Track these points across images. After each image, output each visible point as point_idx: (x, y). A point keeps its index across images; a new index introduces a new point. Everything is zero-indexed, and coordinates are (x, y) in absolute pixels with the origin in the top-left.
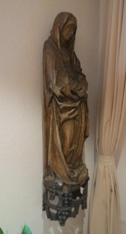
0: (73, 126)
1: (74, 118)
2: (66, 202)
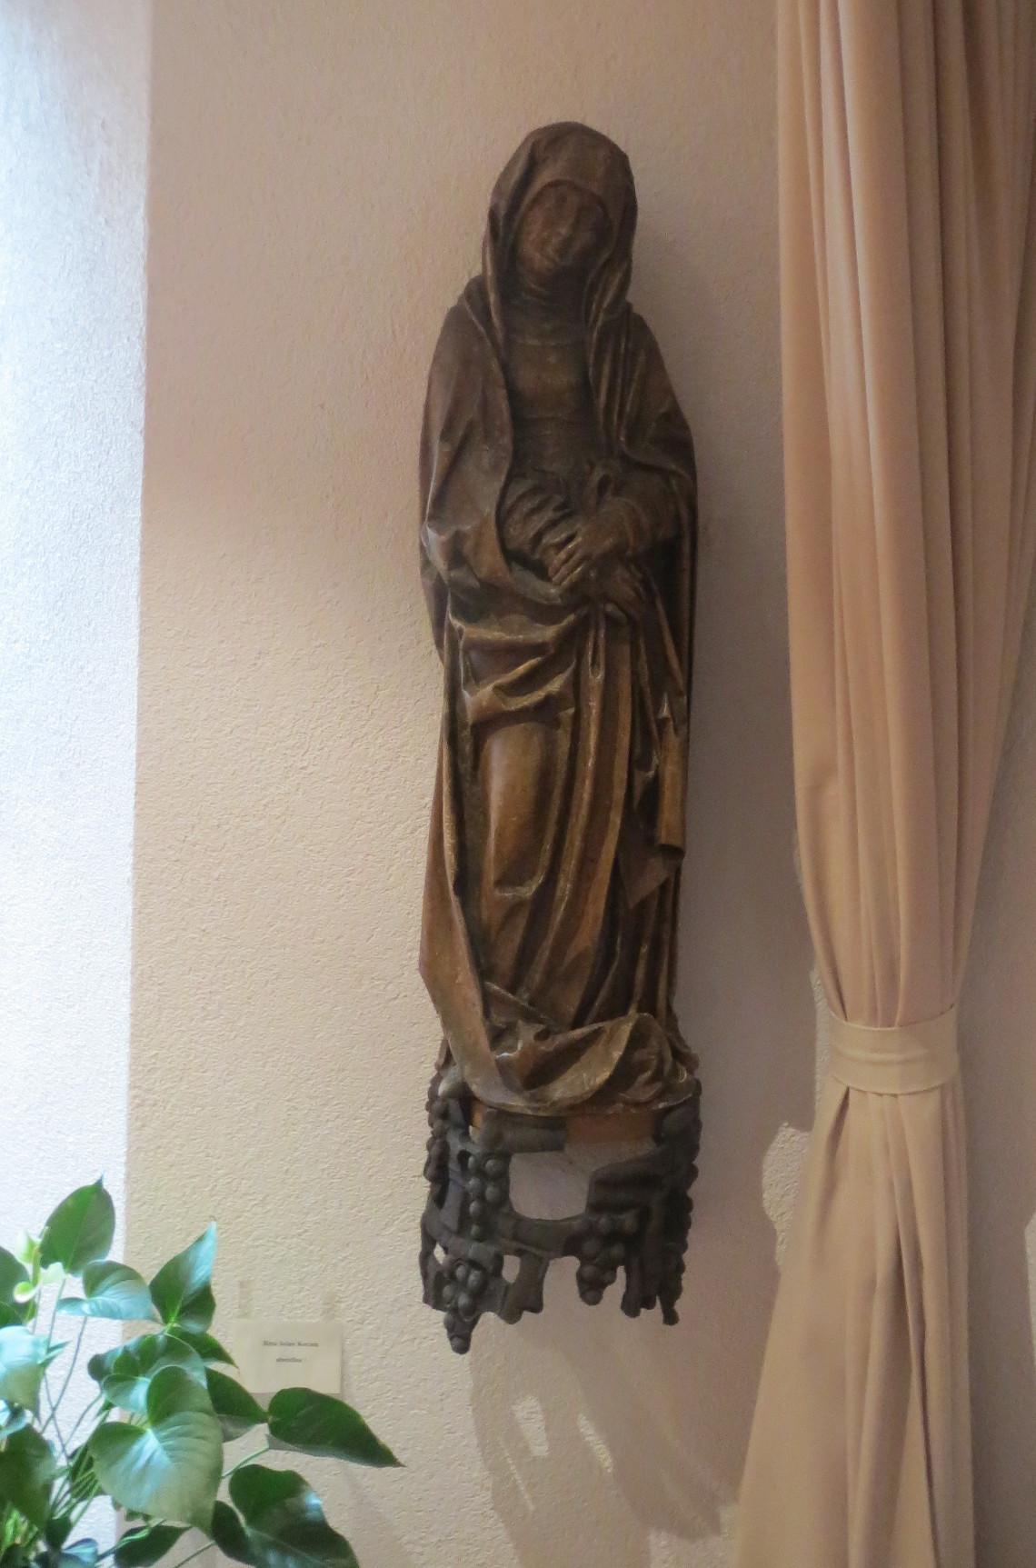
0: (533, 760)
1: (545, 712)
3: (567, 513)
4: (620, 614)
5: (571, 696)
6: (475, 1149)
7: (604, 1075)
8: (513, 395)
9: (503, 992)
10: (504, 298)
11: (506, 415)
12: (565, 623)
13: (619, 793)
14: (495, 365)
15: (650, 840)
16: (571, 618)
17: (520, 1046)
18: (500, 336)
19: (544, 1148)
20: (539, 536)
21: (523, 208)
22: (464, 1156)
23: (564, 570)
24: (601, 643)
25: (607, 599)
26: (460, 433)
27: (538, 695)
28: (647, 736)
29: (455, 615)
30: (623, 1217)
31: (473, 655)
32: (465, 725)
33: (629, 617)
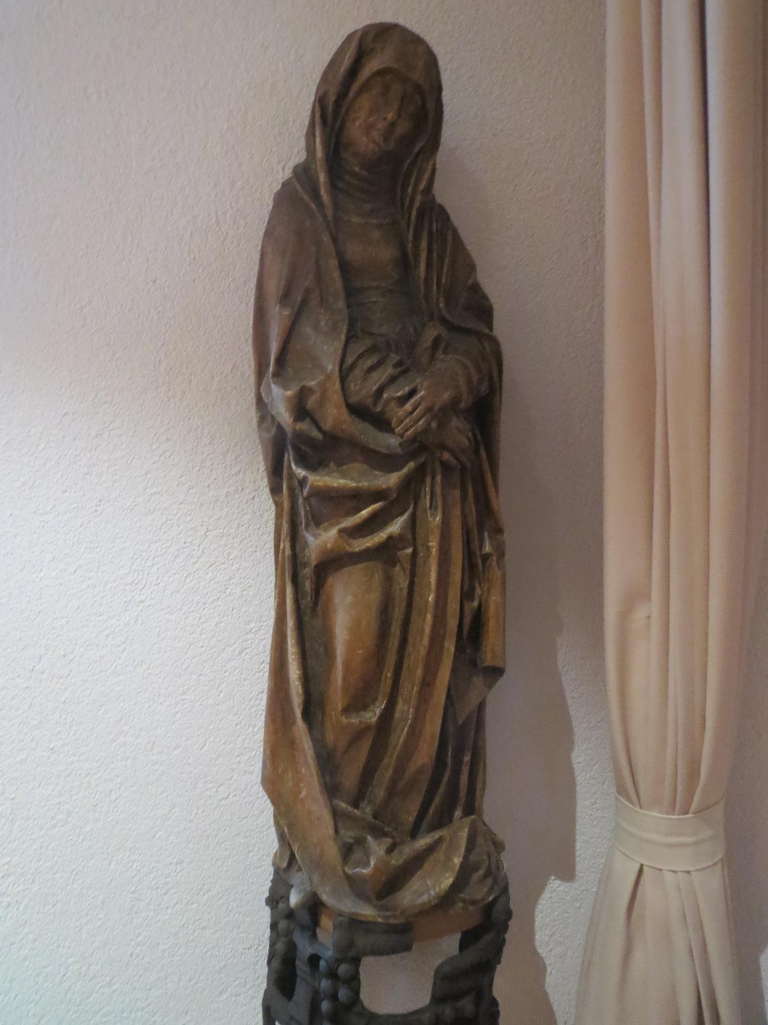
0: (375, 597)
1: (386, 553)
2: (325, 1006)
4: (454, 462)
5: (410, 537)
6: (328, 953)
7: (447, 881)
8: (345, 267)
9: (350, 808)
12: (405, 470)
13: (453, 624)
14: (326, 238)
15: (474, 663)
16: (412, 465)
17: (372, 863)
19: (394, 951)
20: (380, 391)
21: (351, 94)
22: (314, 960)
23: (408, 419)
24: (438, 489)
25: (442, 447)
27: (382, 536)
28: (475, 568)
29: (297, 464)
30: (461, 1003)
31: (313, 501)
32: (305, 565)
33: (463, 468)
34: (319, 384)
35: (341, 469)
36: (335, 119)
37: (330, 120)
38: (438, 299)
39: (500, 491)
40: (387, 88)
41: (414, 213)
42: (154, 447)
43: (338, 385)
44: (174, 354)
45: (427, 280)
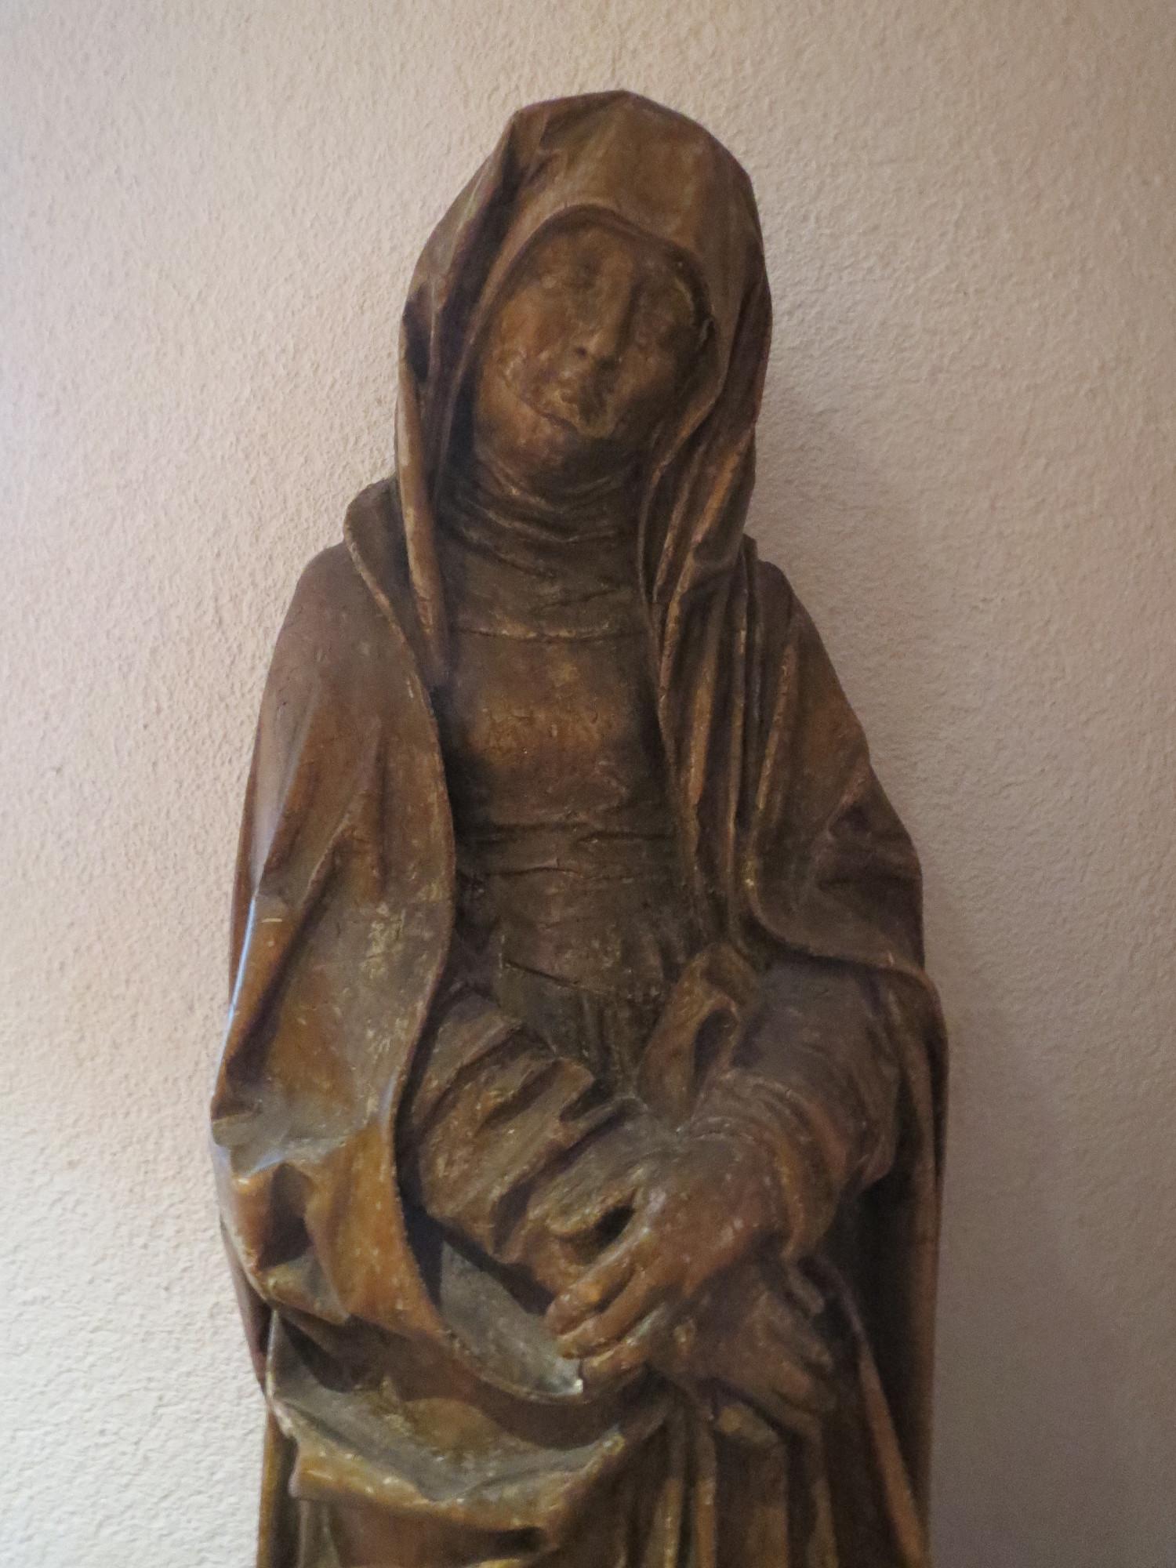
3: (602, 1116)
8: (461, 769)
10: (444, 529)
11: (439, 824)
14: (414, 693)
16: (613, 1443)
18: (429, 617)
21: (489, 291)
25: (719, 1390)
26: (314, 872)
34: (329, 1160)
35: (410, 1405)
36: (449, 363)
37: (434, 362)
38: (739, 863)
39: (935, 1503)
40: (590, 268)
41: (674, 610)
42: (39, 1180)
43: (386, 1172)
44: (98, 948)
45: (709, 802)
